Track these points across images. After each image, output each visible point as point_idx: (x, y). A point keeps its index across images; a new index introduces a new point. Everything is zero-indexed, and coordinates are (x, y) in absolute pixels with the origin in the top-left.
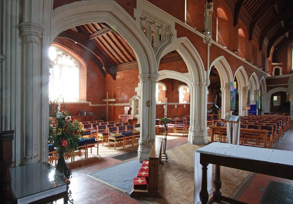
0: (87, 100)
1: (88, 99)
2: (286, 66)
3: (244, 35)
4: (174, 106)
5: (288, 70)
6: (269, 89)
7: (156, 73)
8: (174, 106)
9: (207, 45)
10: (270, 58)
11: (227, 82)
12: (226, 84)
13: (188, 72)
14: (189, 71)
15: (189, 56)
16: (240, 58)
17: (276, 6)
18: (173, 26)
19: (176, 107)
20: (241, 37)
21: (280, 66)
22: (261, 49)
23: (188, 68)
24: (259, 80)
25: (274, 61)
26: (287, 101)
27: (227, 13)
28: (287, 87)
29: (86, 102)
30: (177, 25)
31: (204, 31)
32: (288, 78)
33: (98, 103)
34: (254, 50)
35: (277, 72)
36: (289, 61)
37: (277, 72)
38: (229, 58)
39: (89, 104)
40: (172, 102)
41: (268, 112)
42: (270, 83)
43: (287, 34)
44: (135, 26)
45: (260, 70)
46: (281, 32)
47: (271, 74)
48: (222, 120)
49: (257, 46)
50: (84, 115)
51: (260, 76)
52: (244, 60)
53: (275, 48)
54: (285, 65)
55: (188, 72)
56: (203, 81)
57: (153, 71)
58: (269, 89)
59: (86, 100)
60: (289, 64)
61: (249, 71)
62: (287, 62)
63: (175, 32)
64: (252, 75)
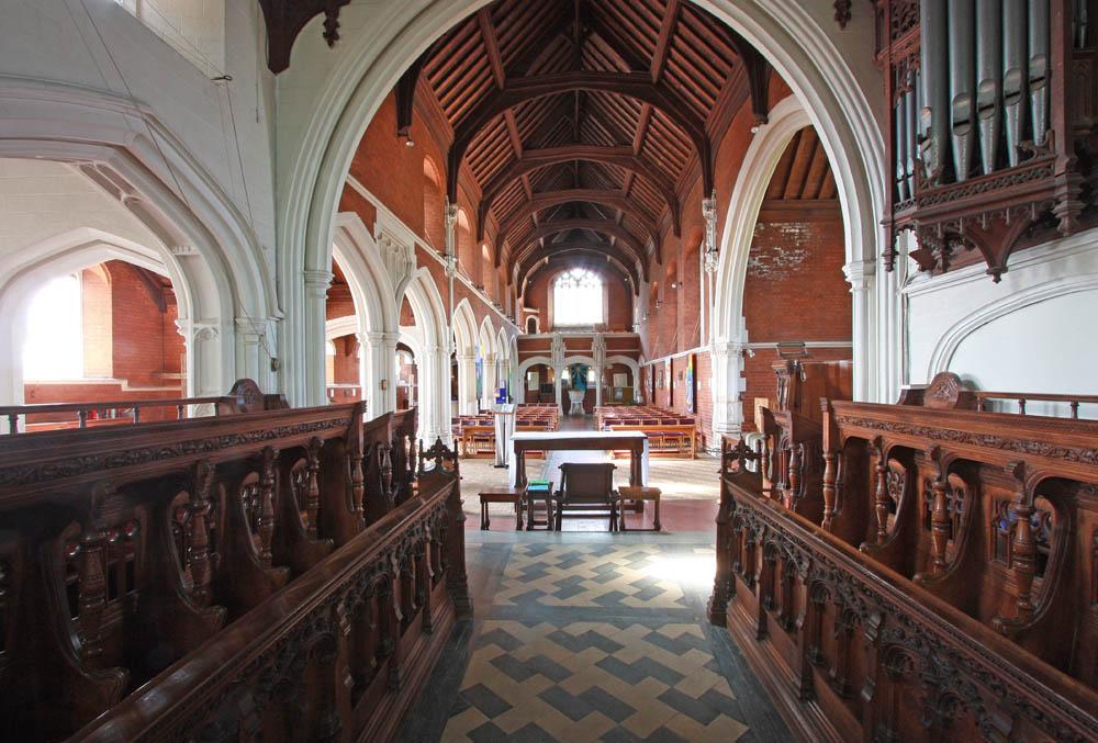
0: (116, 375)
1: (119, 369)
2: (546, 317)
3: (489, 258)
4: (350, 390)
5: (550, 325)
6: (522, 358)
7: (397, 332)
8: (350, 390)
9: (449, 279)
10: (521, 300)
11: (469, 345)
12: (468, 349)
13: (413, 324)
14: (357, 312)
15: (164, 198)
16: (485, 300)
17: (535, 215)
18: (412, 249)
19: (354, 394)
20: (486, 260)
21: (536, 314)
22: (510, 283)
23: (416, 318)
24: (509, 339)
25: (527, 304)
26: (549, 382)
27: (469, 218)
28: (549, 355)
29: (111, 381)
30: (417, 246)
31: (445, 255)
32: (551, 340)
33: (144, 383)
34: (502, 285)
35: (532, 324)
36: (549, 307)
37: (532, 324)
38: (473, 300)
39: (120, 386)
40: (346, 381)
41: (522, 402)
42: (524, 347)
43: (546, 259)
44: (374, 250)
45: (509, 321)
46: (538, 253)
47: (524, 331)
48: (912, 228)
49: (505, 276)
50: (110, 417)
51: (509, 334)
52: (490, 304)
53: (528, 279)
54: (544, 315)
55: (413, 324)
56: (444, 344)
57: (391, 328)
58: (522, 358)
59: (111, 375)
60: (550, 313)
61: (497, 324)
62: (546, 308)
63: (414, 259)
64: (202, 256)
